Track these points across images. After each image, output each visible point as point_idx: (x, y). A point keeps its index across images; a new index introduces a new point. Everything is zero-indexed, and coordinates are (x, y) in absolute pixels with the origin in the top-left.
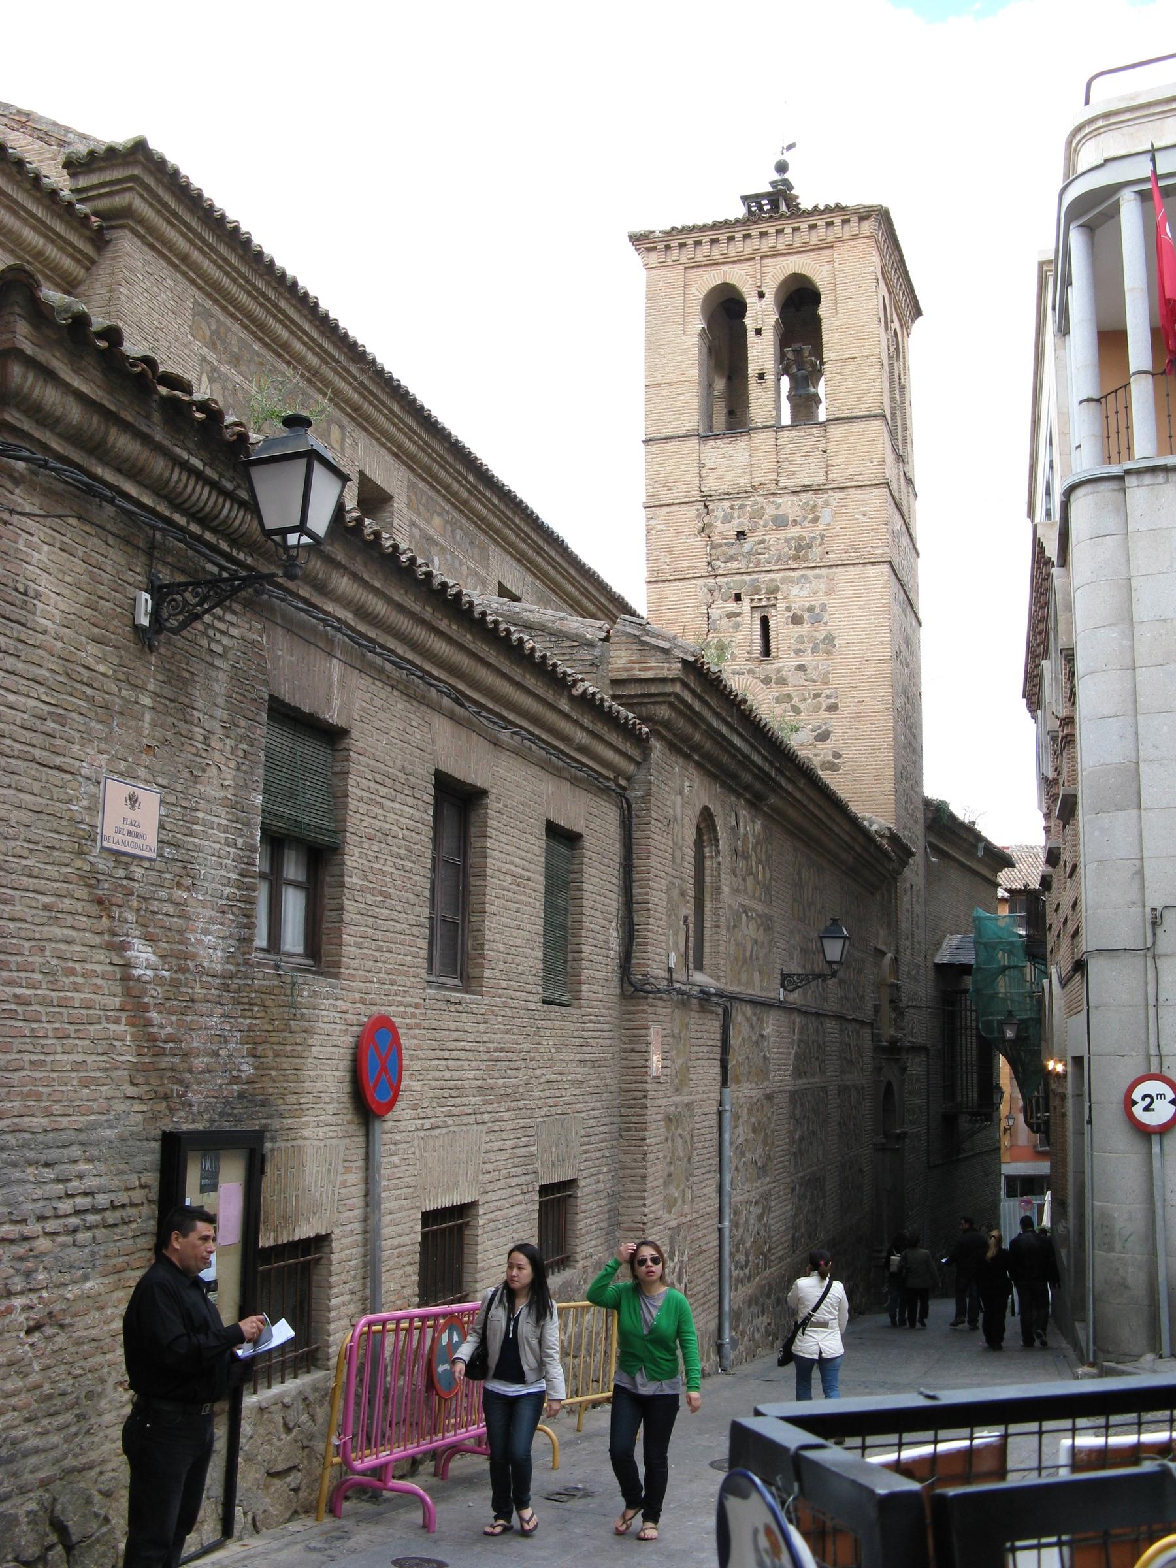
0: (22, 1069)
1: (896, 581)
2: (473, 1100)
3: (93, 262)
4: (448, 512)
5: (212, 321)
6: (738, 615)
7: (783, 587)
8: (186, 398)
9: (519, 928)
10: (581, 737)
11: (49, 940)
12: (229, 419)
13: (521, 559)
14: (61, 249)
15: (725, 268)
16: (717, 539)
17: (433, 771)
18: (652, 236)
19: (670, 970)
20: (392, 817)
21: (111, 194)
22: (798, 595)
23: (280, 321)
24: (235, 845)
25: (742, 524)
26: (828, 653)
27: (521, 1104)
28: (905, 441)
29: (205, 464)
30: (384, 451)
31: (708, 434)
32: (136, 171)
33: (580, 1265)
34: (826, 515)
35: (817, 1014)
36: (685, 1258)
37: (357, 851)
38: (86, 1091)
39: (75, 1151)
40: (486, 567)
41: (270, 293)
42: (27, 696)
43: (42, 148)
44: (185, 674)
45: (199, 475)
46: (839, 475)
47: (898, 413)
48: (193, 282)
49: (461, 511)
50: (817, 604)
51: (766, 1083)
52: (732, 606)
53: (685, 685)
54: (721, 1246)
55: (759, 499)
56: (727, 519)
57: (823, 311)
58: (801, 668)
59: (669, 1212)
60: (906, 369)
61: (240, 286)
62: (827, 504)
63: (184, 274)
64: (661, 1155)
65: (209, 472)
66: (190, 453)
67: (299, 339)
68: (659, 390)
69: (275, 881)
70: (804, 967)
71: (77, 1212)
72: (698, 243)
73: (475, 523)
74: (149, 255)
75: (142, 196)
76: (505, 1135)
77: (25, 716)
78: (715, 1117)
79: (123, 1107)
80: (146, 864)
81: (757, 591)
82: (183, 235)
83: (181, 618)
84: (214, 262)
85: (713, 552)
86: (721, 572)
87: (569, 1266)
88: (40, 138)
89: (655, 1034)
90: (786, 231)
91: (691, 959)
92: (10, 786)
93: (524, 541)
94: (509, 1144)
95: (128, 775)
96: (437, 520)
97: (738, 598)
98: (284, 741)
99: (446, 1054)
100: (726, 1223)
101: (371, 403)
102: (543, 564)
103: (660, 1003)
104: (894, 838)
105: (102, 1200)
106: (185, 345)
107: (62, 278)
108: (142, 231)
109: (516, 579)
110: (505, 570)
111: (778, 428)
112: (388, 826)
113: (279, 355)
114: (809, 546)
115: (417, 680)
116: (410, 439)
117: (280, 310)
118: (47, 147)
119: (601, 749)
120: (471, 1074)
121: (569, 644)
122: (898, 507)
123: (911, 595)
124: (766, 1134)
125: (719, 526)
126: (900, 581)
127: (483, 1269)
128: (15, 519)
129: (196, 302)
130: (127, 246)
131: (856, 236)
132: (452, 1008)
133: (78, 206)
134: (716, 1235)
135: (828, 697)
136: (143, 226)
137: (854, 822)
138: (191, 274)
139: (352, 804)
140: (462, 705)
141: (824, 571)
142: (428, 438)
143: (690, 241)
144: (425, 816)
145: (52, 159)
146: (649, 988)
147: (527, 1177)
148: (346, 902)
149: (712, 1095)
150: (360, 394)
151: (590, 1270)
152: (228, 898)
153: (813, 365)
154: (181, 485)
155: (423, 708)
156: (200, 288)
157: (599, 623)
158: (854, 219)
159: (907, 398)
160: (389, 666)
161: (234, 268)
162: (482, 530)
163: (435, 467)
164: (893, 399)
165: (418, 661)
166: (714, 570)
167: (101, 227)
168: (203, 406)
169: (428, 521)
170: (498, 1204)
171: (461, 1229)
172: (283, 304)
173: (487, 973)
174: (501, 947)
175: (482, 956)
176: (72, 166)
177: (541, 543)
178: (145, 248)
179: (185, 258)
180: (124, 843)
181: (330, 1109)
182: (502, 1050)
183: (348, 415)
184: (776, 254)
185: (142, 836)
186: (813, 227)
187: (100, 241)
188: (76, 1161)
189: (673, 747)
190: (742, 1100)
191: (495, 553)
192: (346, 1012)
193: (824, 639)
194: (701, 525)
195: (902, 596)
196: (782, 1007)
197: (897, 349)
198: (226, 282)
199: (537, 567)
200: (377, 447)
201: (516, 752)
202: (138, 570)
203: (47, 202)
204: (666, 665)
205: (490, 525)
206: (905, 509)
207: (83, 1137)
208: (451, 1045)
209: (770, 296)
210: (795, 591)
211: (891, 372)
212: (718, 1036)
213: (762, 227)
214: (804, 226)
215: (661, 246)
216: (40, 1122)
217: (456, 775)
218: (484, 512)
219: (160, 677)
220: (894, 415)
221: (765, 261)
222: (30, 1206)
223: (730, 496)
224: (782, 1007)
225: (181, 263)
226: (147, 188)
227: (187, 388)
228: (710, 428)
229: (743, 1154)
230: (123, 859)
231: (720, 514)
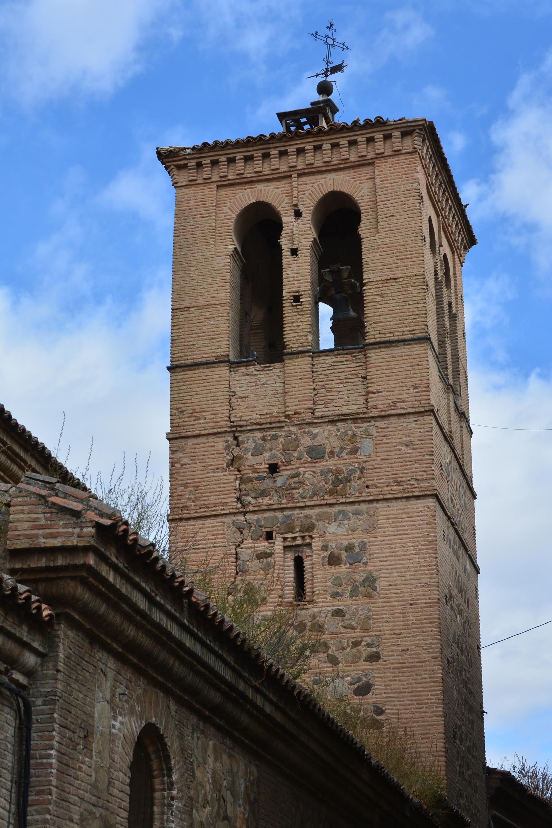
1: (445, 518)
6: (270, 555)
7: (320, 524)
15: (260, 186)
18: (182, 153)
25: (274, 457)
26: (369, 596)
28: (456, 372)
34: (366, 445)
47: (448, 341)
52: (262, 545)
55: (293, 429)
56: (258, 451)
57: (364, 230)
58: (339, 613)
62: (368, 435)
72: (231, 161)
81: (291, 530)
85: (243, 487)
86: (251, 508)
90: (324, 147)
97: (269, 536)
122: (448, 439)
123: (466, 537)
125: (250, 459)
126: (449, 518)
131: (397, 153)
135: (369, 645)
141: (363, 507)
143: (223, 159)
153: (353, 286)
158: (396, 133)
159: (459, 328)
164: (440, 326)
166: (244, 506)
177: (16, 448)
193: (364, 581)
197: (447, 273)
204: (77, 530)
206: (456, 443)
209: (307, 215)
210: (332, 528)
213: (299, 143)
214: (344, 142)
215: (192, 163)
220: (442, 344)
221: (302, 179)
223: (260, 427)
231: (250, 445)
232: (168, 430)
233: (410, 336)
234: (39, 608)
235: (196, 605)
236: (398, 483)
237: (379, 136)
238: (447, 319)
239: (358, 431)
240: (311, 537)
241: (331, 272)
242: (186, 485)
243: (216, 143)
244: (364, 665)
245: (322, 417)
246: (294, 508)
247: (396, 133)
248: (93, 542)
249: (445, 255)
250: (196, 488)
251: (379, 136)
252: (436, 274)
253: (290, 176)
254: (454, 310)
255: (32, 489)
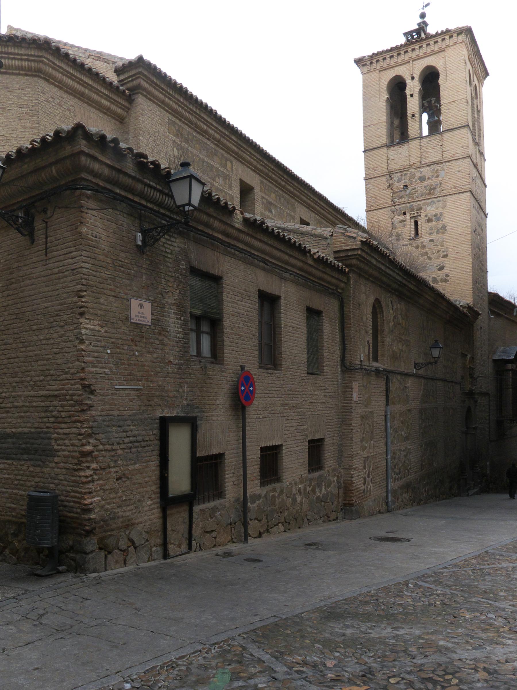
0: (109, 395)
2: (279, 408)
3: (129, 109)
4: (277, 191)
5: (176, 126)
7: (424, 207)
8: (145, 161)
9: (296, 346)
10: (320, 274)
11: (115, 353)
12: (163, 166)
13: (308, 207)
14: (117, 106)
15: (397, 68)
16: (395, 189)
17: (257, 290)
19: (361, 361)
20: (241, 307)
21: (132, 80)
22: (430, 210)
23: (203, 122)
24: (180, 319)
26: (443, 233)
27: (299, 410)
28: (480, 135)
29: (156, 184)
30: (249, 170)
31: (391, 144)
32: (140, 70)
33: (326, 469)
34: (442, 173)
35: (432, 379)
36: (371, 469)
37: (228, 320)
38: (131, 403)
39: (129, 422)
40: (295, 212)
41: (197, 111)
42: (100, 272)
43: (107, 66)
44: (157, 261)
45: (155, 189)
46: (448, 155)
47: (476, 123)
48: (167, 111)
49: (283, 191)
50: (438, 213)
51: (407, 405)
52: (402, 217)
53: (363, 250)
54: (387, 465)
55: (413, 170)
56: (399, 181)
57: (441, 81)
58: (432, 240)
59: (363, 451)
60: (481, 102)
61: (185, 110)
62: (443, 169)
63: (164, 109)
64: (359, 430)
65: (158, 187)
66: (150, 181)
67: (211, 128)
68: (369, 128)
69: (199, 333)
70: (426, 360)
71: (131, 442)
72: (384, 59)
73: (289, 195)
74: (150, 103)
75: (143, 79)
76: (293, 421)
77: (100, 279)
78: (383, 417)
79: (145, 408)
80: (148, 327)
81: (413, 210)
82: (161, 93)
83: (153, 240)
84: (174, 102)
86: (397, 203)
87: (322, 470)
88: (106, 62)
89: (355, 386)
91: (371, 357)
92: (97, 303)
93: (309, 199)
94: (295, 424)
95: (139, 297)
96: (273, 195)
98: (196, 282)
99: (268, 392)
100: (389, 457)
101: (242, 151)
102: (318, 208)
103: (357, 374)
104: (469, 308)
105: (139, 438)
106: (166, 137)
107: (119, 117)
108: (145, 93)
109: (307, 215)
110: (302, 212)
111: (421, 137)
112: (240, 311)
113: (203, 136)
114: (435, 188)
115: (249, 257)
116: (259, 163)
117: (202, 118)
118: (108, 65)
119: (326, 277)
120: (278, 399)
121: (317, 239)
122: (475, 166)
123: (482, 204)
124: (408, 425)
126: (476, 199)
127: (286, 468)
128: (90, 211)
129: (169, 119)
130: (140, 100)
131: (456, 43)
132: (269, 375)
133: (121, 88)
134: (385, 461)
135: (443, 252)
136: (146, 92)
137: (449, 303)
138: (166, 108)
139: (225, 303)
140: (267, 265)
141: (441, 198)
142: (266, 162)
144: (255, 306)
145: (111, 70)
146: (352, 368)
147: (303, 437)
148: (225, 338)
149: (382, 409)
150: (238, 148)
151: (331, 471)
152: (179, 338)
153: (436, 107)
154: (149, 193)
155: (252, 267)
156: (170, 113)
157: (329, 229)
160: (237, 252)
161: (182, 103)
162: (292, 197)
163: (270, 174)
164: (473, 117)
165: (249, 250)
166: (394, 203)
167: (129, 94)
168: (153, 163)
169: (269, 196)
170: (291, 446)
171: (276, 454)
172: (203, 115)
173: (283, 363)
174: (289, 354)
175: (281, 357)
176: (118, 71)
178: (148, 100)
179: (163, 102)
180: (139, 320)
181: (222, 410)
182: (291, 390)
183: (234, 157)
184: (419, 58)
185: (146, 318)
186: (436, 42)
187: (130, 100)
188: (129, 426)
189: (360, 275)
190: (396, 411)
191: (297, 205)
192: (227, 377)
193: (442, 227)
194: (388, 184)
195: (477, 205)
196: (416, 376)
197: (476, 93)
198: (180, 109)
199: (316, 209)
200: (246, 168)
201: (292, 281)
202: (136, 225)
203: (109, 88)
205: (295, 195)
206: (479, 167)
207: (132, 418)
208: (270, 389)
209: (417, 78)
210: (429, 208)
211: (473, 105)
212: (384, 387)
213: (412, 47)
214: (432, 43)
215: (368, 63)
216: (116, 413)
217: (267, 291)
218: (292, 190)
219: (148, 262)
220: (474, 125)
221: (414, 62)
222: (115, 439)
224: (416, 376)
225: (162, 104)
226: (145, 76)
227: (145, 157)
228: (392, 141)
229: (397, 432)
230: (140, 326)
232: (364, 176)
233: (460, 125)
234: (345, 269)
235: (391, 259)
236: (455, 187)
237: (447, 37)
238: (476, 114)
239: (439, 168)
240: (421, 212)
241: (428, 102)
242: (371, 197)
243: (378, 52)
244: (442, 259)
245: (424, 164)
246: (414, 202)
247: (455, 35)
248: (360, 247)
249: (475, 85)
250: (376, 198)
251: (447, 37)
252: (472, 94)
253: (409, 62)
254: (479, 108)
255: (340, 231)
